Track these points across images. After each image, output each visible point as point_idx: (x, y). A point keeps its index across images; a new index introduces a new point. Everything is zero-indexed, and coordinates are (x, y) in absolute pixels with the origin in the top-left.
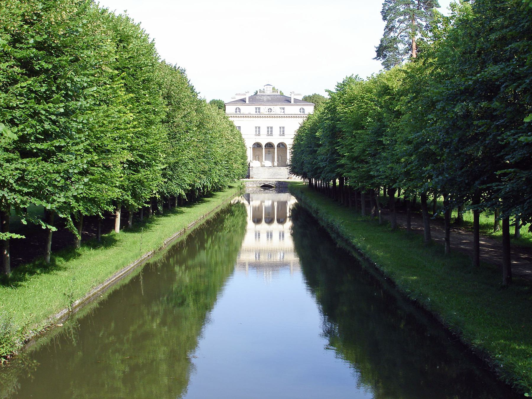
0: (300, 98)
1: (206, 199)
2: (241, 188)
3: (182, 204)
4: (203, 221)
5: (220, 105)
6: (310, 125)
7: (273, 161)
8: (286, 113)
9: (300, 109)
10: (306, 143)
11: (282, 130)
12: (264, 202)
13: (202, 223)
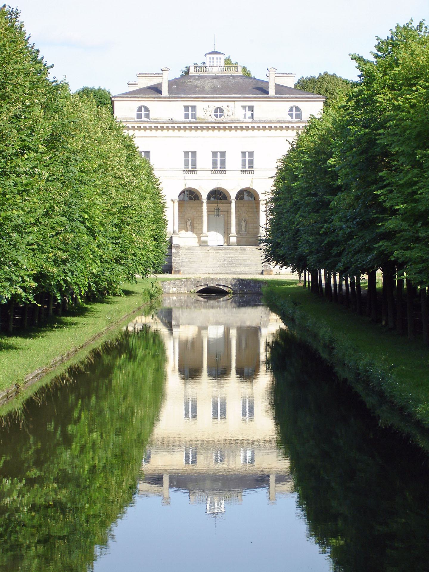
0: (291, 83)
1: (69, 319)
2: (151, 296)
3: (11, 328)
4: (62, 370)
5: (103, 100)
6: (314, 142)
7: (227, 233)
8: (257, 117)
9: (291, 110)
10: (305, 185)
11: (247, 159)
12: (206, 328)
13: (58, 374)
